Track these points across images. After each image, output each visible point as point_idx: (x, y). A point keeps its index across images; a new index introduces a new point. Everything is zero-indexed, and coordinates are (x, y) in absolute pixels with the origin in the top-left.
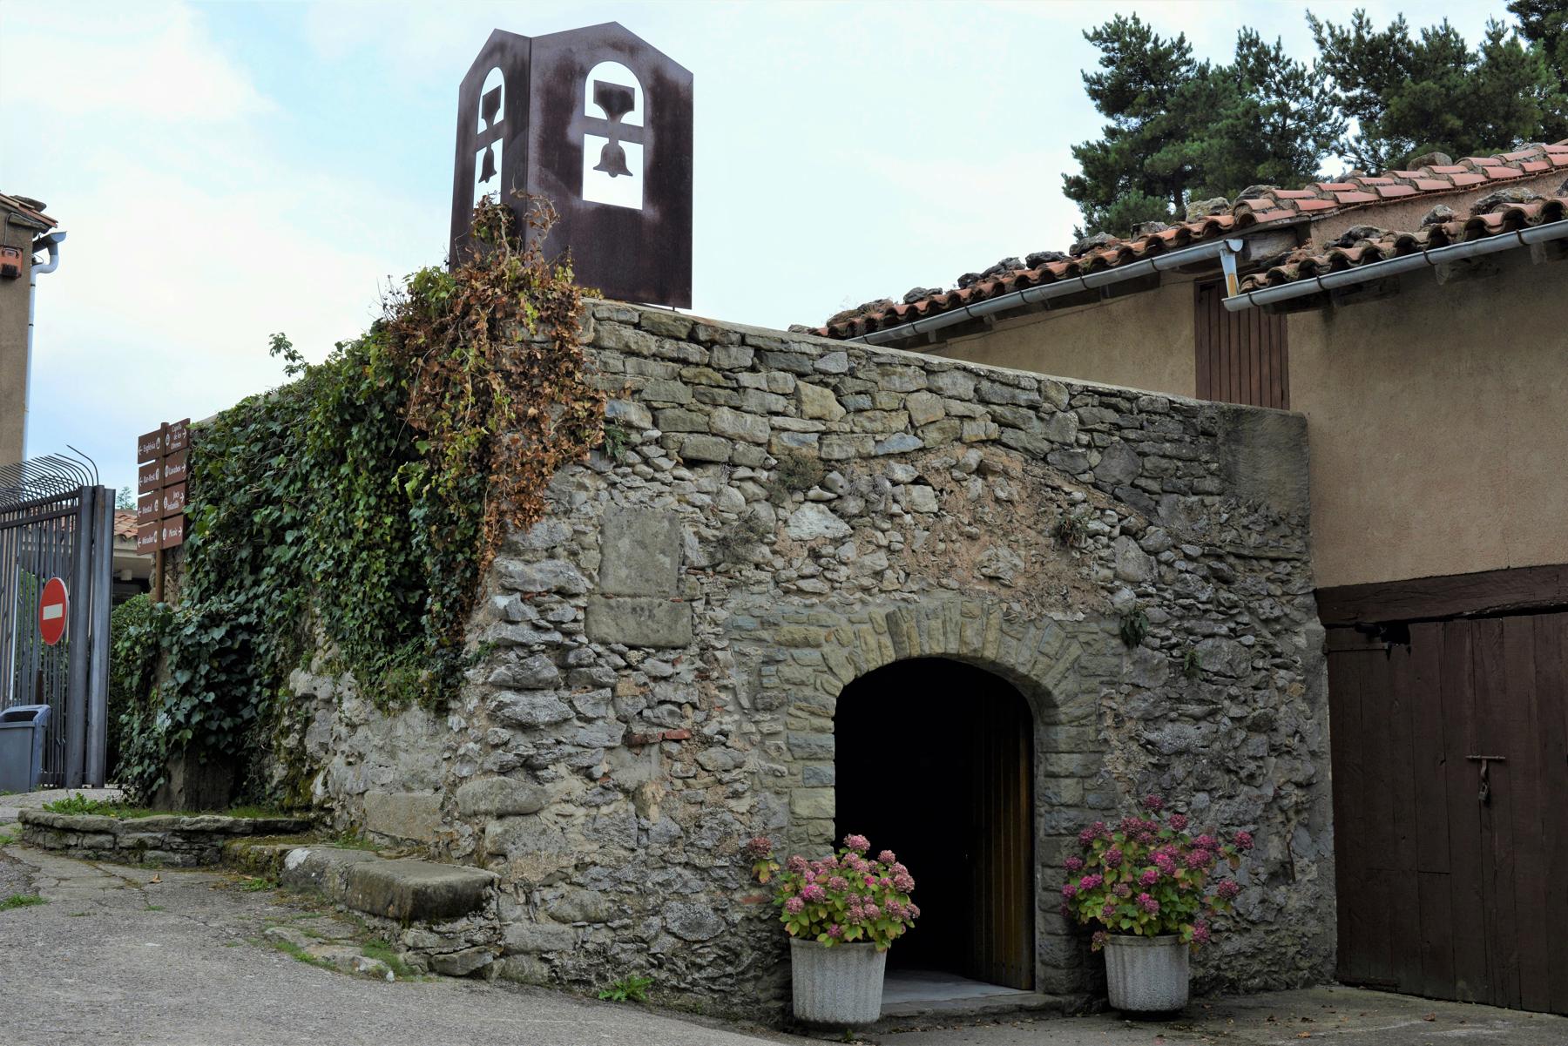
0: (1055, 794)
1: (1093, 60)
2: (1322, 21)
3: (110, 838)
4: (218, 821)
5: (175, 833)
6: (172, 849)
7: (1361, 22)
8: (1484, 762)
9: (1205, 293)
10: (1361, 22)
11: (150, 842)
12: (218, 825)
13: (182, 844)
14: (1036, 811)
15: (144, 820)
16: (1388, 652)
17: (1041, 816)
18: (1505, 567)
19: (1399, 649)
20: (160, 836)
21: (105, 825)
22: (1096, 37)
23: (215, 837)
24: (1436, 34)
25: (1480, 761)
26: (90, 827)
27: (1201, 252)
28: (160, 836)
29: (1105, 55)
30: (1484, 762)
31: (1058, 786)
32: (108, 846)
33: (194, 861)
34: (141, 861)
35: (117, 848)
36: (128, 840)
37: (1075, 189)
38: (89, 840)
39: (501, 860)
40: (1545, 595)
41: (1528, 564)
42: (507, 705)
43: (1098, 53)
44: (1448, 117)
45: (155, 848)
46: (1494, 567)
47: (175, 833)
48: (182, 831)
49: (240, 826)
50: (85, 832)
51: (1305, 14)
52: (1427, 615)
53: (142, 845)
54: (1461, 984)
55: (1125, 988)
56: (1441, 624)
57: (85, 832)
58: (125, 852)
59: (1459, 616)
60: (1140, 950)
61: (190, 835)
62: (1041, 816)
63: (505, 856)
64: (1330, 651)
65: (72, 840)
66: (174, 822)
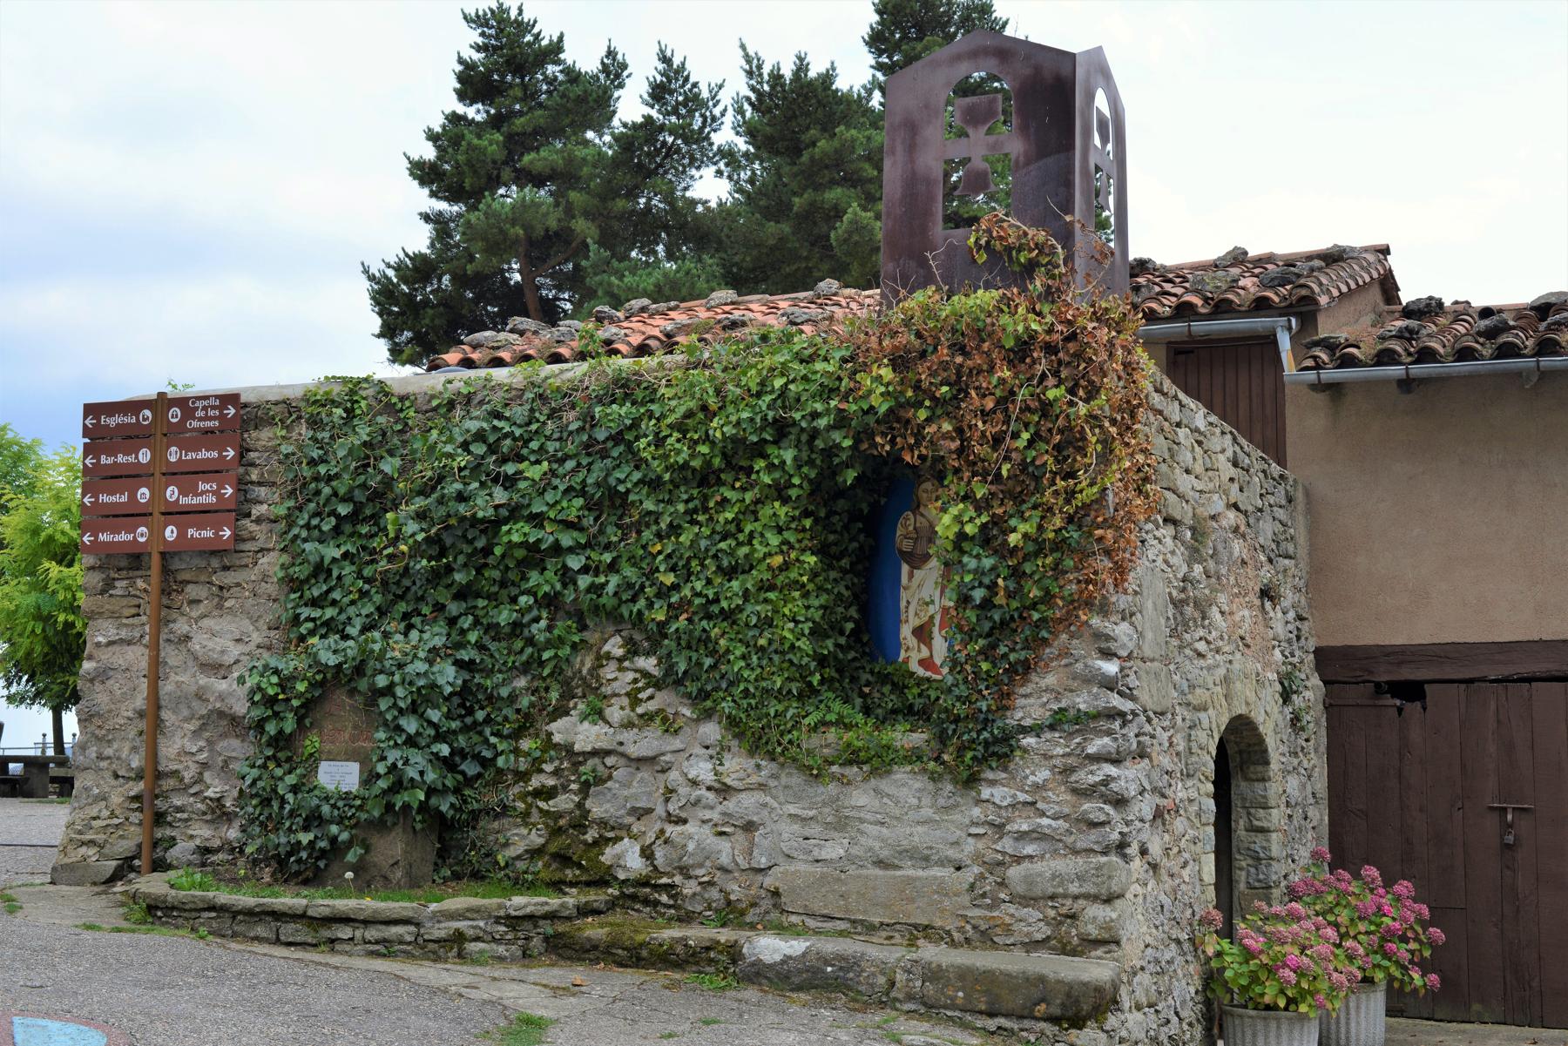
0: (1264, 848)
1: (466, 42)
2: (752, 53)
3: (412, 928)
4: (547, 903)
5: (498, 920)
6: (494, 940)
7: (802, 66)
8: (1510, 811)
9: (1181, 358)
10: (802, 66)
11: (471, 932)
12: (546, 908)
13: (506, 933)
14: (1236, 864)
15: (245, 899)
16: (1400, 710)
17: (1241, 869)
18: (1536, 639)
19: (1414, 708)
20: (482, 924)
21: (411, 914)
22: (477, 21)
23: (541, 923)
24: (776, 77)
25: (1505, 810)
26: (383, 917)
27: (1254, 325)
28: (482, 924)
29: (480, 40)
30: (1510, 811)
31: (1268, 841)
32: (409, 938)
33: (519, 953)
34: (460, 955)
35: (420, 941)
36: (441, 931)
37: (424, 173)
38: (373, 933)
39: (1113, 947)
40: (1525, 669)
41: (1562, 637)
42: (1114, 779)
43: (475, 36)
44: (479, 118)
45: (477, 939)
46: (1525, 639)
47: (498, 920)
48: (508, 917)
49: (568, 908)
50: (366, 923)
51: (738, 44)
52: (1447, 677)
53: (459, 938)
54: (1476, 1007)
55: (1348, 1032)
56: (1463, 686)
57: (366, 923)
58: (431, 946)
59: (1483, 680)
60: (1363, 996)
61: (513, 922)
62: (1241, 869)
63: (1118, 943)
64: (1331, 705)
65: (345, 932)
66: (500, 907)
